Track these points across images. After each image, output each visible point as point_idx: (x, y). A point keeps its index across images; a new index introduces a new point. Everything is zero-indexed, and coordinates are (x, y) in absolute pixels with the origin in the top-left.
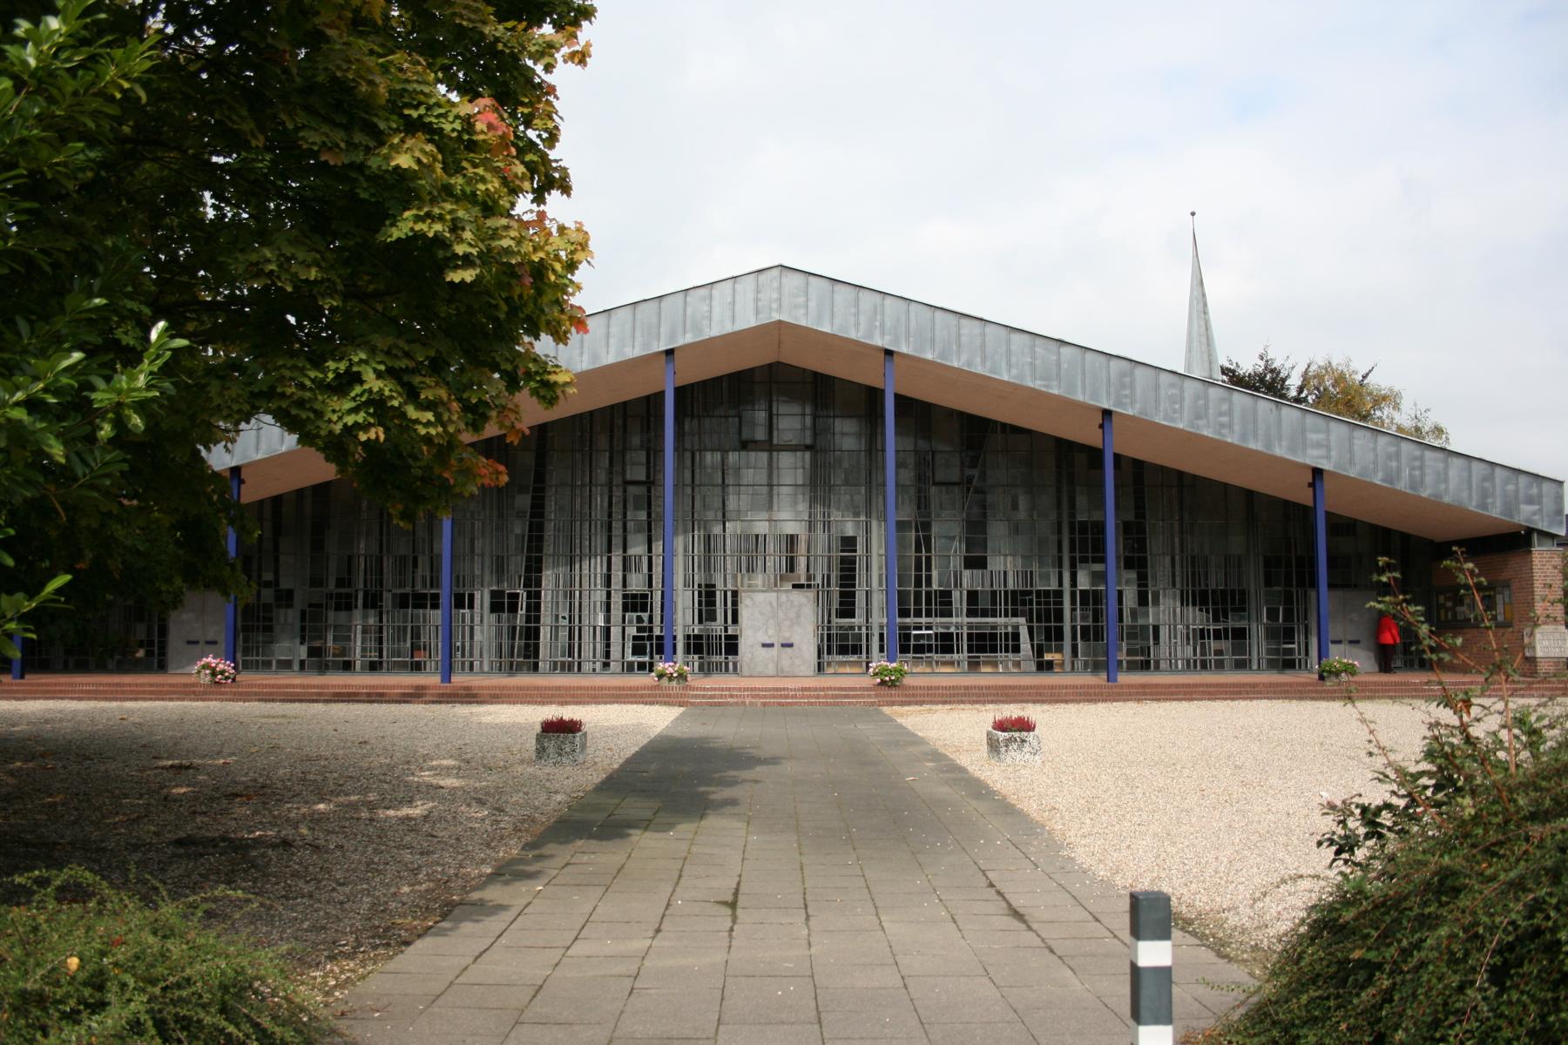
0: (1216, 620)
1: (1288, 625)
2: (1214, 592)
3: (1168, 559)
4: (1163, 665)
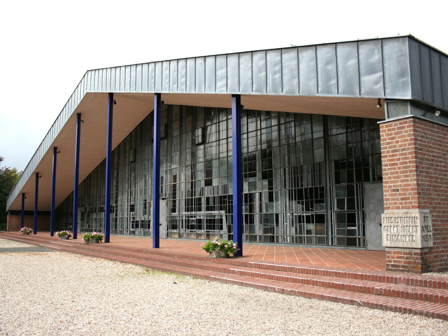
0: (307, 209)
1: (351, 211)
2: (306, 189)
3: (282, 170)
4: (280, 240)
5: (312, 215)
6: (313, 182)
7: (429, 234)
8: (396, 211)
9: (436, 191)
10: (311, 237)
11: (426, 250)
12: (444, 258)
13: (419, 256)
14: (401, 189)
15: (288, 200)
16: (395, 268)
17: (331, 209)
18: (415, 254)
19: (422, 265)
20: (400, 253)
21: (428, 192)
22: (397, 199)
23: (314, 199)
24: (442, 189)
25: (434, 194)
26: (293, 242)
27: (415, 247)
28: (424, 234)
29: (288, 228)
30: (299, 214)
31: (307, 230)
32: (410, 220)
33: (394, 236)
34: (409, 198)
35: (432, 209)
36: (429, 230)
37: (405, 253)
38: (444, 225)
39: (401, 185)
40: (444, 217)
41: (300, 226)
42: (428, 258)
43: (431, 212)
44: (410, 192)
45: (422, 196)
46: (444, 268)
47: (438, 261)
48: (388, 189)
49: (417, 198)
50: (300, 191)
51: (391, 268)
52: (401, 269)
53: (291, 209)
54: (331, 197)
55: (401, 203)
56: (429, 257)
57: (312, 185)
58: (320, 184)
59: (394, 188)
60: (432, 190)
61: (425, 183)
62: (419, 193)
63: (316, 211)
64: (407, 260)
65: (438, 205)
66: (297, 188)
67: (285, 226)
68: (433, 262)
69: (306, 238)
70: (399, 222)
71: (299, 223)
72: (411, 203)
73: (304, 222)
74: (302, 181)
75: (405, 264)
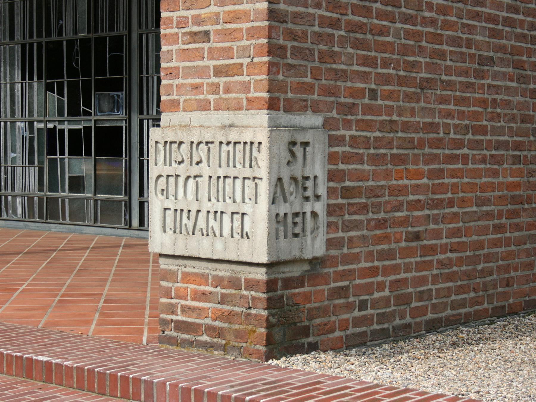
0: (74, 111)
2: (71, 43)
5: (87, 129)
6: (93, 23)
7: (308, 208)
8: (197, 117)
9: (358, 44)
10: (83, 199)
11: (295, 271)
12: (377, 295)
13: (261, 295)
14: (217, 32)
15: (18, 78)
16: (185, 336)
17: (141, 113)
18: (251, 285)
19: (269, 326)
20: (203, 278)
21: (324, 48)
22: (202, 72)
23: (92, 78)
24: (390, 39)
25: (351, 56)
26: (31, 214)
27: (249, 260)
28: (283, 209)
29: (19, 171)
30: (50, 126)
31: (70, 178)
32: (239, 155)
33: (185, 215)
34: (238, 69)
35: (334, 114)
36: (309, 193)
37: (219, 282)
38: (387, 175)
39: (217, 15)
40: (389, 144)
41: (53, 163)
42: (299, 299)
43: (328, 124)
44: (245, 42)
45: (290, 61)
46: (374, 333)
47: (349, 307)
48: (175, 30)
49: (265, 69)
50: (54, 49)
51: (173, 334)
52: (205, 338)
53: (27, 107)
54: (141, 72)
55: (214, 89)
56: (307, 297)
57: (89, 32)
58: (111, 29)
59: (196, 29)
60: (342, 41)
61: (311, 10)
62: (273, 50)
63: (99, 117)
64: (224, 307)
65: (366, 101)
66: (44, 40)
67: (9, 164)
68: (324, 311)
69: (67, 201)
70: (204, 163)
71: (49, 154)
72: (245, 87)
73: (62, 153)
74: (60, 18)
75: (217, 323)
